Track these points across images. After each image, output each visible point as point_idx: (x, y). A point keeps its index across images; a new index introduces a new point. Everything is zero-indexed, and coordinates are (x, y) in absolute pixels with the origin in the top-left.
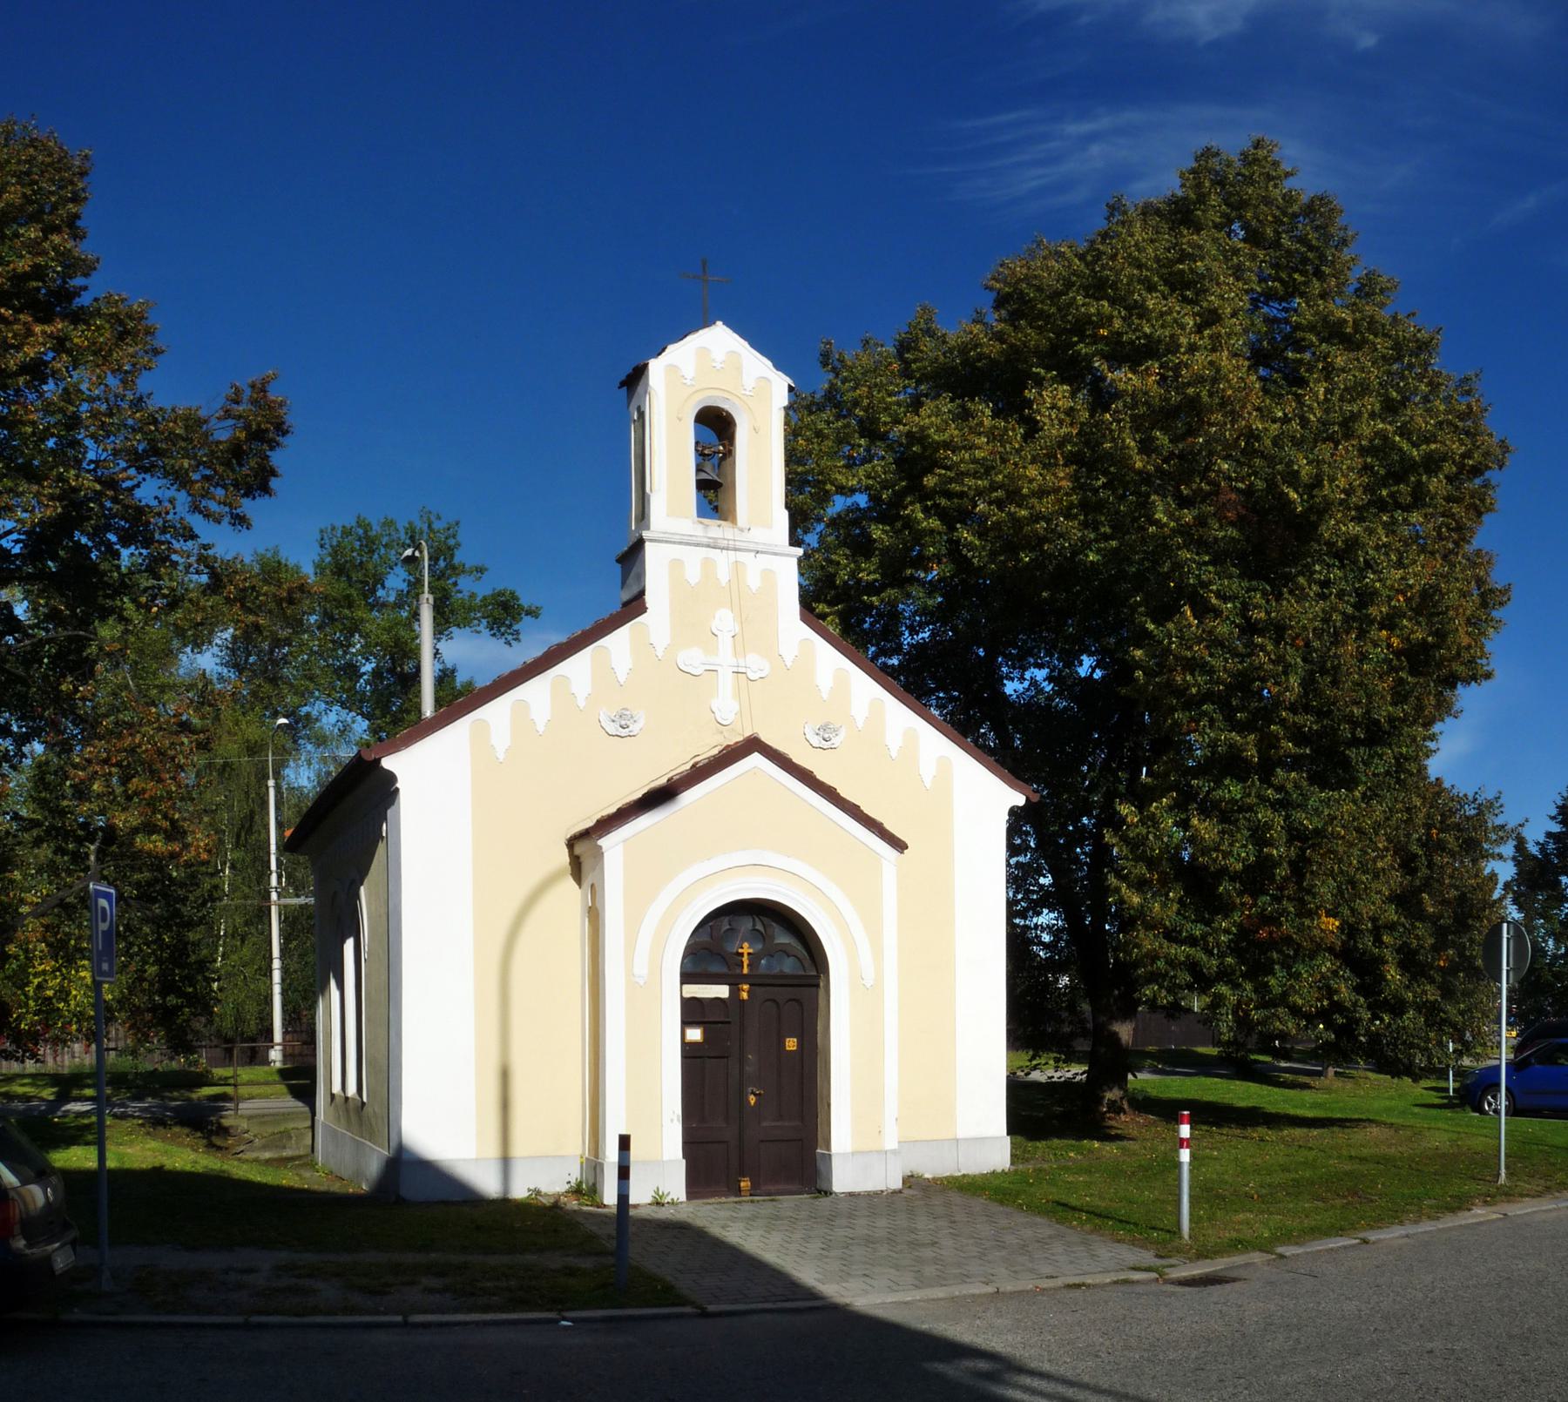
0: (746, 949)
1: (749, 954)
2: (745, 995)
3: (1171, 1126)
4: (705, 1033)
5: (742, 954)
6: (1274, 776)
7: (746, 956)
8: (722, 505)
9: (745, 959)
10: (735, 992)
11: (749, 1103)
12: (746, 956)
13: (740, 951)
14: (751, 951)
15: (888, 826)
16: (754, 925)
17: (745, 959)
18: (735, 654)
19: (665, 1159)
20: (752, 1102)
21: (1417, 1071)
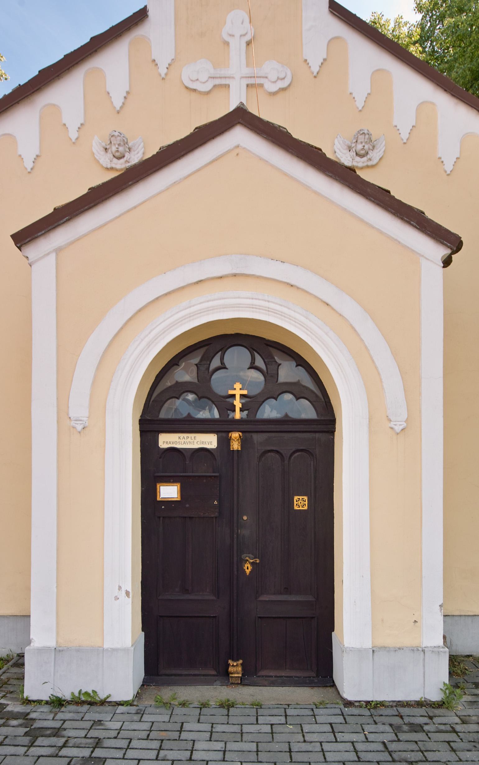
0: (238, 390)
1: (242, 396)
2: (236, 446)
3: (242, 106)
4: (182, 491)
5: (233, 396)
6: (424, 60)
7: (238, 397)
8: (22, 248)
9: (238, 404)
10: (224, 442)
11: (244, 571)
12: (238, 397)
13: (231, 392)
14: (245, 392)
15: (430, 214)
16: (253, 359)
17: (238, 404)
18: (248, 65)
19: (106, 646)
20: (248, 572)
21: (474, 82)
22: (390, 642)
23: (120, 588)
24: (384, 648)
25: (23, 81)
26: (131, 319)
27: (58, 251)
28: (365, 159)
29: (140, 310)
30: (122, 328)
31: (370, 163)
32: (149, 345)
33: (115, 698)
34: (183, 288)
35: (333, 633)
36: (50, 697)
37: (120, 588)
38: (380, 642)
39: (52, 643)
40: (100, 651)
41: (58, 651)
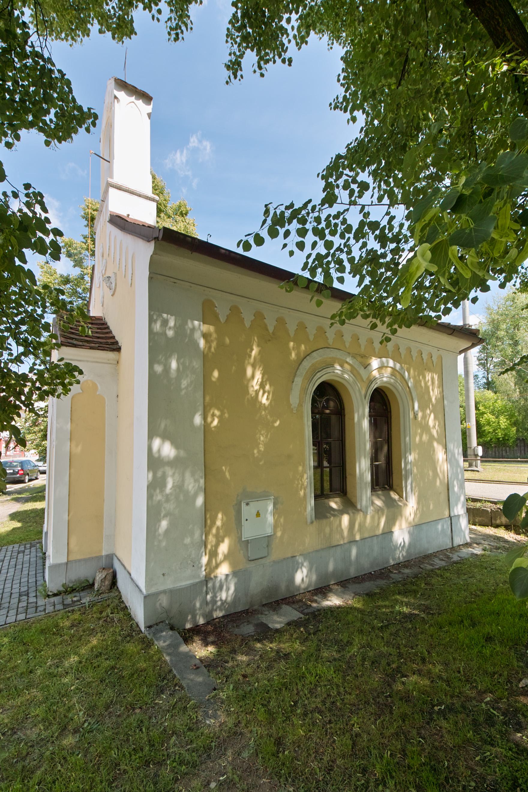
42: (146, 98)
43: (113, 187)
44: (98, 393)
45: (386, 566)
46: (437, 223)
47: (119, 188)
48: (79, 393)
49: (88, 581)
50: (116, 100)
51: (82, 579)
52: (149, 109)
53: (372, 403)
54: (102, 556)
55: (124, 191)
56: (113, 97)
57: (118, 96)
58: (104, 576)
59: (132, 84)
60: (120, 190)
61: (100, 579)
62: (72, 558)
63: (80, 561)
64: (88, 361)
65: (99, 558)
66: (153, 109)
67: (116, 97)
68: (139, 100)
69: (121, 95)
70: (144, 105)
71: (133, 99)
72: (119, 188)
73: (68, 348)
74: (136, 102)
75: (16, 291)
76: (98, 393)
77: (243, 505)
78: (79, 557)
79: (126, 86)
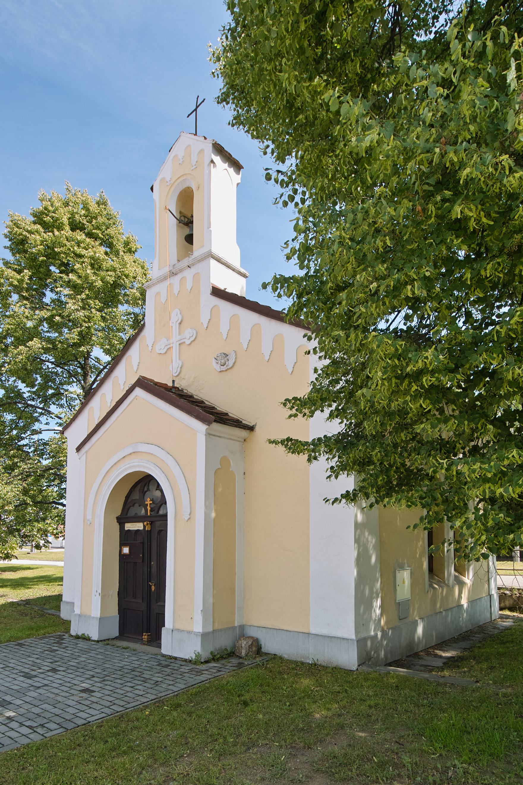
19: (92, 616)
22: (181, 627)
23: (97, 591)
24: (178, 630)
25: (261, 303)
26: (105, 476)
27: (86, 452)
28: (225, 366)
29: (107, 472)
30: (102, 480)
31: (228, 367)
32: (109, 487)
33: (92, 639)
34: (120, 460)
35: (163, 628)
36: (64, 505)
37: (97, 591)
38: (178, 626)
39: (79, 613)
40: (90, 617)
41: (80, 616)
42: (237, 166)
43: (214, 258)
44: (231, 469)
45: (461, 632)
46: (351, 307)
47: (219, 260)
48: (219, 469)
49: (226, 649)
50: (212, 165)
51: (224, 648)
52: (237, 178)
53: (165, 512)
54: (236, 627)
55: (222, 263)
56: (210, 160)
57: (215, 161)
58: (250, 643)
59: (229, 151)
60: (219, 262)
61: (247, 646)
62: (215, 628)
63: (221, 630)
64: (225, 438)
65: (233, 628)
66: (241, 179)
67: (212, 161)
68: (231, 168)
69: (217, 159)
70: (234, 173)
71: (226, 165)
72: (219, 260)
73: (218, 424)
74: (228, 169)
75: (49, 347)
76: (231, 469)
77: (397, 572)
78: (220, 627)
79: (221, 151)
